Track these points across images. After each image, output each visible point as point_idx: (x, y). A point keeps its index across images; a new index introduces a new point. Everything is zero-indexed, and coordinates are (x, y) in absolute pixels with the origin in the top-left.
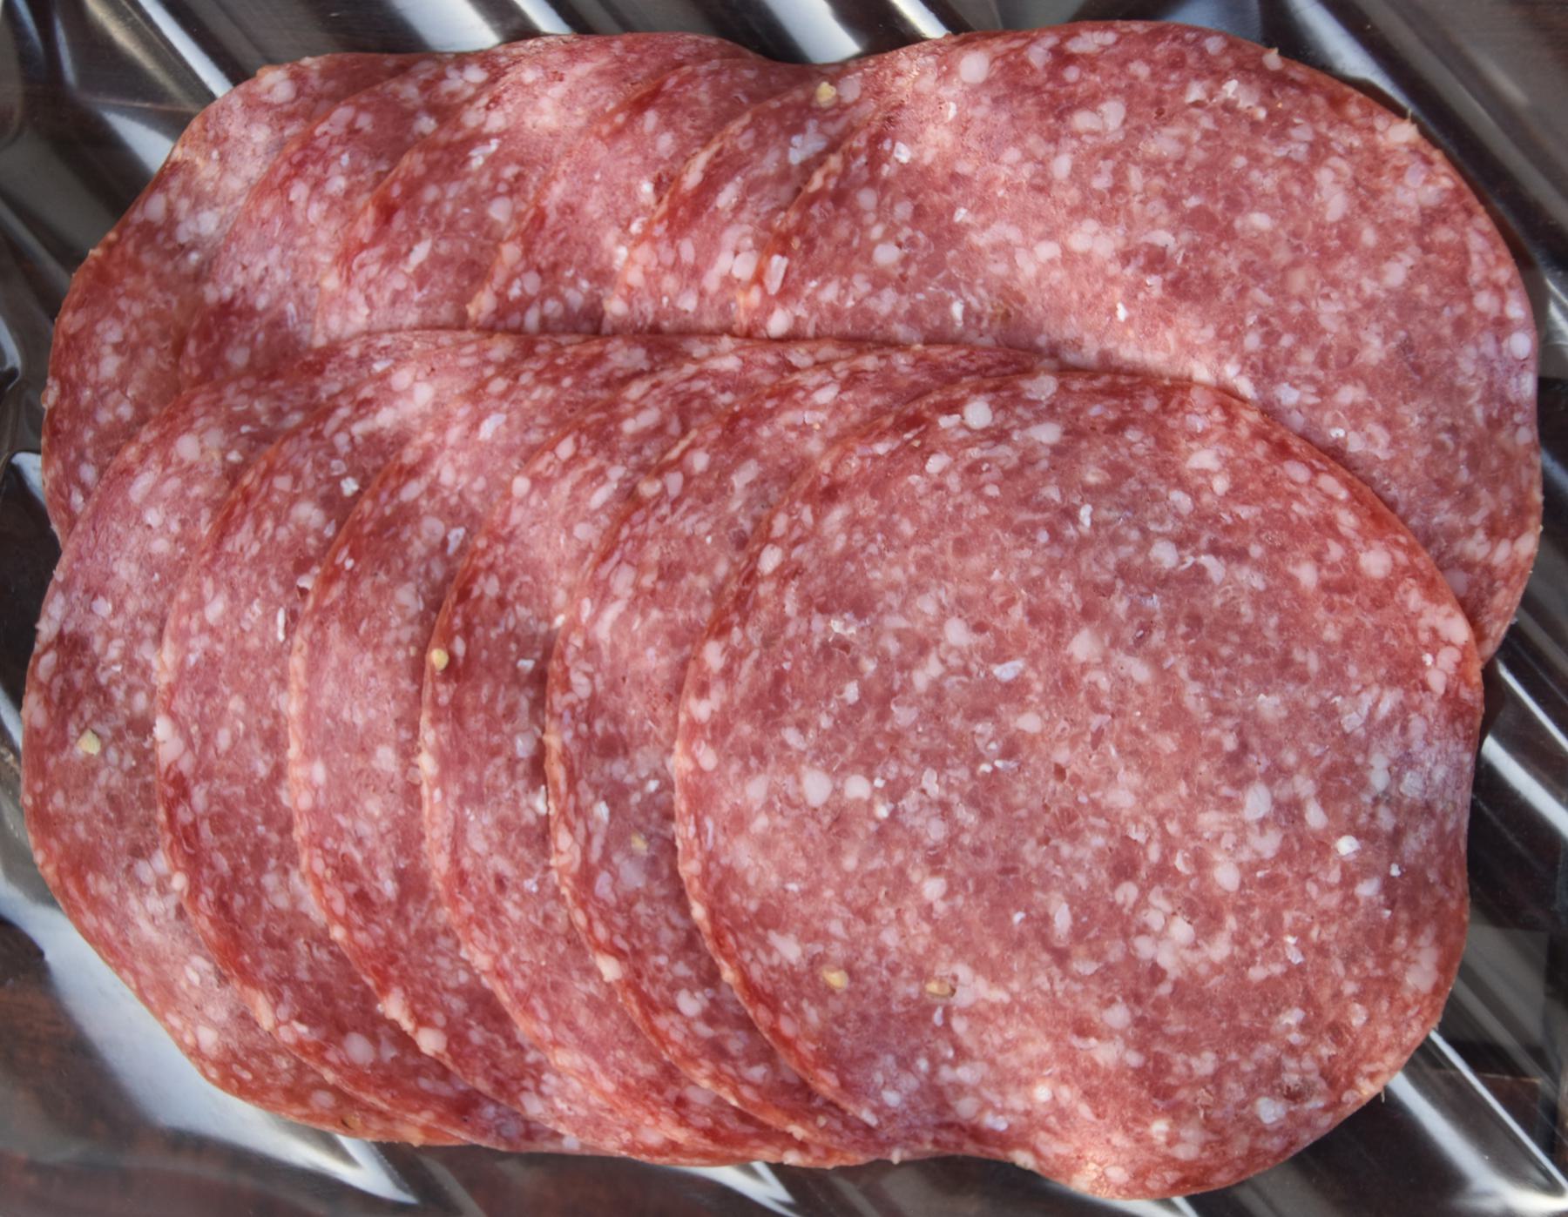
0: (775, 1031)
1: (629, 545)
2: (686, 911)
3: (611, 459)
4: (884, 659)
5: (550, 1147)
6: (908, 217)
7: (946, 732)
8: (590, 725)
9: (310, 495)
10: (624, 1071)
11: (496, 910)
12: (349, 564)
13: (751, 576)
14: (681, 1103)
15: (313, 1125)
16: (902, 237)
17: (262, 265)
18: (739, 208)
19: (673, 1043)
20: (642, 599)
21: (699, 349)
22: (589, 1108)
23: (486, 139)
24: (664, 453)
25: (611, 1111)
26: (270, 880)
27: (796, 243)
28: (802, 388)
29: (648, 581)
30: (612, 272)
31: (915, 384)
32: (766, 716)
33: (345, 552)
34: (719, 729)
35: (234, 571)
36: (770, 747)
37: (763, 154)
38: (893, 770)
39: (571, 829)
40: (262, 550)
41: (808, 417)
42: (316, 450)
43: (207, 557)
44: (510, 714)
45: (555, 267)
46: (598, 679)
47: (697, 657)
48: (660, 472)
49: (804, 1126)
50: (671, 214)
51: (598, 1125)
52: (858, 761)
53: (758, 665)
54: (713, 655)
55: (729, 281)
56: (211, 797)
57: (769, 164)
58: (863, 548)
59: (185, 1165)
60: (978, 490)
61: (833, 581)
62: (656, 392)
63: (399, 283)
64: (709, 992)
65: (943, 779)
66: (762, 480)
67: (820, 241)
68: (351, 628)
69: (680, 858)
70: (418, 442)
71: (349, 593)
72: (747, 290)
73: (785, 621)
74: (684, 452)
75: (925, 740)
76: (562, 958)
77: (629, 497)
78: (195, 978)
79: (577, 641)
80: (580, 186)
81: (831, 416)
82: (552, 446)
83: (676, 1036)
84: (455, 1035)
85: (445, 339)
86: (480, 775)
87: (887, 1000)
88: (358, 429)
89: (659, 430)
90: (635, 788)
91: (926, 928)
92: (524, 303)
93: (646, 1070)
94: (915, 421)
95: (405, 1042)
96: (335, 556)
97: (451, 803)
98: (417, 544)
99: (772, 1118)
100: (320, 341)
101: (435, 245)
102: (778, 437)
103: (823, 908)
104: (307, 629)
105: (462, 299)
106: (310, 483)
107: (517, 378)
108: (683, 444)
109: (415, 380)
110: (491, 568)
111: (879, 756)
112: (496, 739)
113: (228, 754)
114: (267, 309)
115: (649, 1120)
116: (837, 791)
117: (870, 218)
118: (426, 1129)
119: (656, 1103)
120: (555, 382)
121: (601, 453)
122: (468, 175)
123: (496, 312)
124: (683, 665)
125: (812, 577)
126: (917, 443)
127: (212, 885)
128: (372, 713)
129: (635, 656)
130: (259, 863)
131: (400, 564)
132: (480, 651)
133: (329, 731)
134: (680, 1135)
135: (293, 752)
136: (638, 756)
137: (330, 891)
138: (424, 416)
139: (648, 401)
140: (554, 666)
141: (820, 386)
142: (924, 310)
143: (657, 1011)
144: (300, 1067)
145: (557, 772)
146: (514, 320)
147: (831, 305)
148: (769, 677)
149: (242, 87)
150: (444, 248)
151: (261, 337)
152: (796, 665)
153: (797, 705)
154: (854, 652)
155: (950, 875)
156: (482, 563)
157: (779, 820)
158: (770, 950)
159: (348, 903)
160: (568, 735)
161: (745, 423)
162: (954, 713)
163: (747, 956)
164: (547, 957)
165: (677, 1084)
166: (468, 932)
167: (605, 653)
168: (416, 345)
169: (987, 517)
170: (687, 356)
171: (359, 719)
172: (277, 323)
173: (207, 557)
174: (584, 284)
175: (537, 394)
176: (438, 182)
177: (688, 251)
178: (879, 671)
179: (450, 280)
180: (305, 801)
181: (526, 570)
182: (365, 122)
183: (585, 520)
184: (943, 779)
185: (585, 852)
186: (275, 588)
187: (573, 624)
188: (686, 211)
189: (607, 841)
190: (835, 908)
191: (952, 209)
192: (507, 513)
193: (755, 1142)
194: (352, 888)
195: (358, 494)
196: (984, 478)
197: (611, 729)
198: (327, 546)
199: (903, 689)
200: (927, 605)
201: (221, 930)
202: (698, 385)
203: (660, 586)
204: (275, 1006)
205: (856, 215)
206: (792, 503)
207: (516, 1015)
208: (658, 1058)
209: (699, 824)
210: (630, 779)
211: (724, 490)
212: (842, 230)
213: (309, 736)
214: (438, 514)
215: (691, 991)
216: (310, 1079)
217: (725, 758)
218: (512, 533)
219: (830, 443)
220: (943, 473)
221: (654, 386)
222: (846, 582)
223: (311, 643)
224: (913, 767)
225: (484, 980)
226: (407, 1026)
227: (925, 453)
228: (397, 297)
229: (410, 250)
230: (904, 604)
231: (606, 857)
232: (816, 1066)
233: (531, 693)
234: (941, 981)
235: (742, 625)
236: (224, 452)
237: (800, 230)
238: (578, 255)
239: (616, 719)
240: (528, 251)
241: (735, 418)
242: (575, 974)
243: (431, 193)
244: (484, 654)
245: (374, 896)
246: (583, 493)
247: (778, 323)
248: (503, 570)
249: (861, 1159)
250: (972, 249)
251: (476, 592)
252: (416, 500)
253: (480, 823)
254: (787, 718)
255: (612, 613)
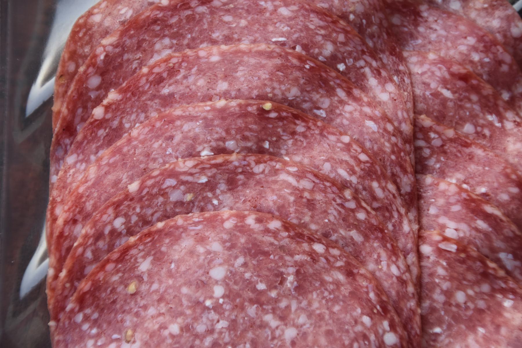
0: (108, 261)
1: (322, 186)
2: (159, 220)
3: (360, 177)
4: (276, 301)
5: (52, 169)
6: (478, 307)
7: (245, 331)
8: (241, 173)
9: (337, 50)
10: (88, 196)
11: (157, 137)
12: (307, 67)
13: (311, 240)
14: (75, 221)
15: (61, 63)
16: (470, 304)
17: (438, 28)
18: (477, 230)
19: (101, 216)
20: (298, 193)
21: (412, 215)
22: (71, 183)
23: (501, 121)
24: (364, 200)
25: (70, 192)
26: (167, 41)
27: (463, 255)
28: (397, 260)
29: (306, 195)
30: (444, 178)
31: (402, 310)
32: (249, 250)
33: (312, 65)
34: (241, 228)
35: (301, 18)
36: (235, 251)
37: (502, 241)
38: (227, 307)
39: (195, 166)
40: (312, 30)
41: (384, 263)
42: (357, 52)
43: (307, 7)
44: (245, 138)
45: (445, 152)
46: (262, 176)
47: (273, 217)
48: (355, 198)
49: (66, 276)
50: (473, 200)
51: (63, 187)
52: (230, 291)
53: (272, 244)
54: (275, 225)
55: (443, 227)
56: (202, 15)
57: (498, 243)
58: (326, 289)
59: (40, 17)
60: (356, 339)
61: (311, 276)
62: (391, 196)
63: (433, 85)
64: (124, 232)
65: (224, 330)
66: (354, 244)
67: (464, 266)
68: (279, 68)
69: (184, 215)
70: (363, 95)
71: (294, 67)
72: (440, 234)
73: (292, 255)
74: (365, 209)
75: (241, 321)
76: (138, 166)
77: (343, 186)
78: (122, 12)
79: (278, 166)
80: (482, 161)
81: (385, 273)
82: (364, 151)
83: (105, 218)
84: (101, 123)
85: (410, 105)
86: (217, 126)
87: (124, 312)
88: (367, 70)
89: (374, 198)
90: (214, 195)
91: (156, 327)
92: (428, 140)
93: (89, 206)
94: (385, 310)
95: (98, 102)
96: (311, 61)
97: (205, 114)
98: (318, 96)
99: (68, 262)
100: (405, 54)
101: (451, 100)
102: (374, 249)
103: (164, 280)
104: (278, 50)
105: (428, 113)
106: (342, 50)
107: (394, 135)
108: (369, 208)
109: (390, 93)
110: (309, 128)
111: (233, 300)
112: (233, 132)
113: (221, 21)
114: (418, 32)
115: (66, 208)
116: (217, 282)
117: (477, 289)
118: (59, 112)
119: (74, 210)
120: (393, 152)
121: (362, 172)
122: (484, 114)
123: (423, 127)
124: (269, 212)
125: (312, 266)
126: (375, 311)
127: (164, 16)
128: (242, 79)
129: (273, 191)
130: (172, 36)
131: (308, 89)
132: (270, 126)
133: (233, 62)
134: (60, 222)
135: (224, 47)
136: (228, 195)
137: (163, 66)
138: (375, 97)
139: (387, 193)
140: (267, 157)
141: (398, 267)
142: (436, 315)
143: (115, 209)
144: (85, 57)
145: (220, 160)
146: (420, 135)
147: (436, 272)
148: (266, 249)
149: (517, 14)
150: (450, 104)
151: (406, 29)
152: (272, 261)
153: (254, 262)
154: (279, 287)
155: (180, 336)
156: (310, 124)
157: (202, 257)
158: (144, 257)
159: (158, 74)
160: (236, 163)
161: (380, 235)
162: (254, 334)
163: (141, 247)
164: (138, 160)
165: (83, 220)
166: (147, 125)
167: (274, 178)
168: (406, 93)
169: (344, 344)
170: (408, 211)
171: (239, 74)
172: (412, 36)
173: (307, 7)
174: (438, 166)
175: (387, 144)
176: (480, 101)
177: (456, 208)
178: (272, 298)
179: (436, 107)
180: (202, 54)
181: (308, 143)
182: (505, 68)
183: (332, 167)
184: (224, 330)
185: (185, 173)
186: (296, 36)
187: (285, 164)
188: (473, 206)
189: (191, 183)
190: (164, 285)
191: (484, 326)
192: (333, 134)
193: (58, 255)
194: (165, 75)
195: (339, 71)
196: (361, 342)
197: (240, 182)
198: (314, 58)
199: (263, 310)
200: (302, 319)
201: (144, 21)
202: (396, 215)
203: (304, 200)
204: (111, 45)
205: (477, 283)
206: (345, 257)
207: (111, 148)
208: (94, 211)
209: (199, 222)
210: (218, 192)
211: (349, 226)
212: (470, 276)
213: (231, 53)
214: (331, 105)
215: (124, 224)
216: (80, 61)
217: (229, 232)
218: (325, 136)
219: (373, 273)
220: (363, 324)
221: (394, 195)
222: (311, 283)
223: (272, 52)
224: (229, 316)
225: (126, 134)
226: (105, 102)
227: (371, 315)
228: (427, 85)
229: (448, 89)
230: (302, 309)
231: (183, 183)
232: (93, 281)
233: (254, 147)
234: (133, 336)
235: (289, 237)
236: (354, 13)
237: (469, 257)
238: (450, 162)
239: (244, 185)
240: (451, 140)
241: (382, 231)
242: (130, 173)
243: (474, 98)
244: (270, 126)
245: (162, 84)
246: (344, 165)
247: (426, 249)
248: (308, 133)
249: (50, 307)
250: (466, 336)
251: (297, 122)
252: (337, 95)
253: (195, 128)
254: (248, 258)
255: (292, 180)
